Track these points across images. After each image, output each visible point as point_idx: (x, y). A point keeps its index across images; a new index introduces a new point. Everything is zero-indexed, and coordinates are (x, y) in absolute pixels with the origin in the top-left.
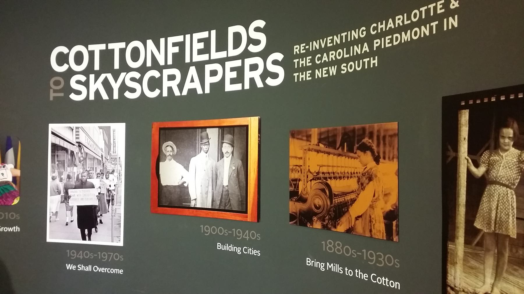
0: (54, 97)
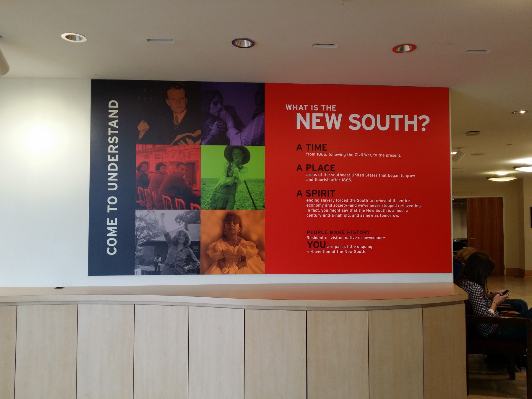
0: (110, 211)
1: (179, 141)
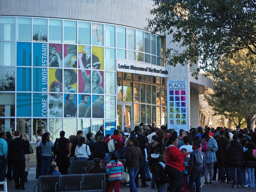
1: (88, 67)
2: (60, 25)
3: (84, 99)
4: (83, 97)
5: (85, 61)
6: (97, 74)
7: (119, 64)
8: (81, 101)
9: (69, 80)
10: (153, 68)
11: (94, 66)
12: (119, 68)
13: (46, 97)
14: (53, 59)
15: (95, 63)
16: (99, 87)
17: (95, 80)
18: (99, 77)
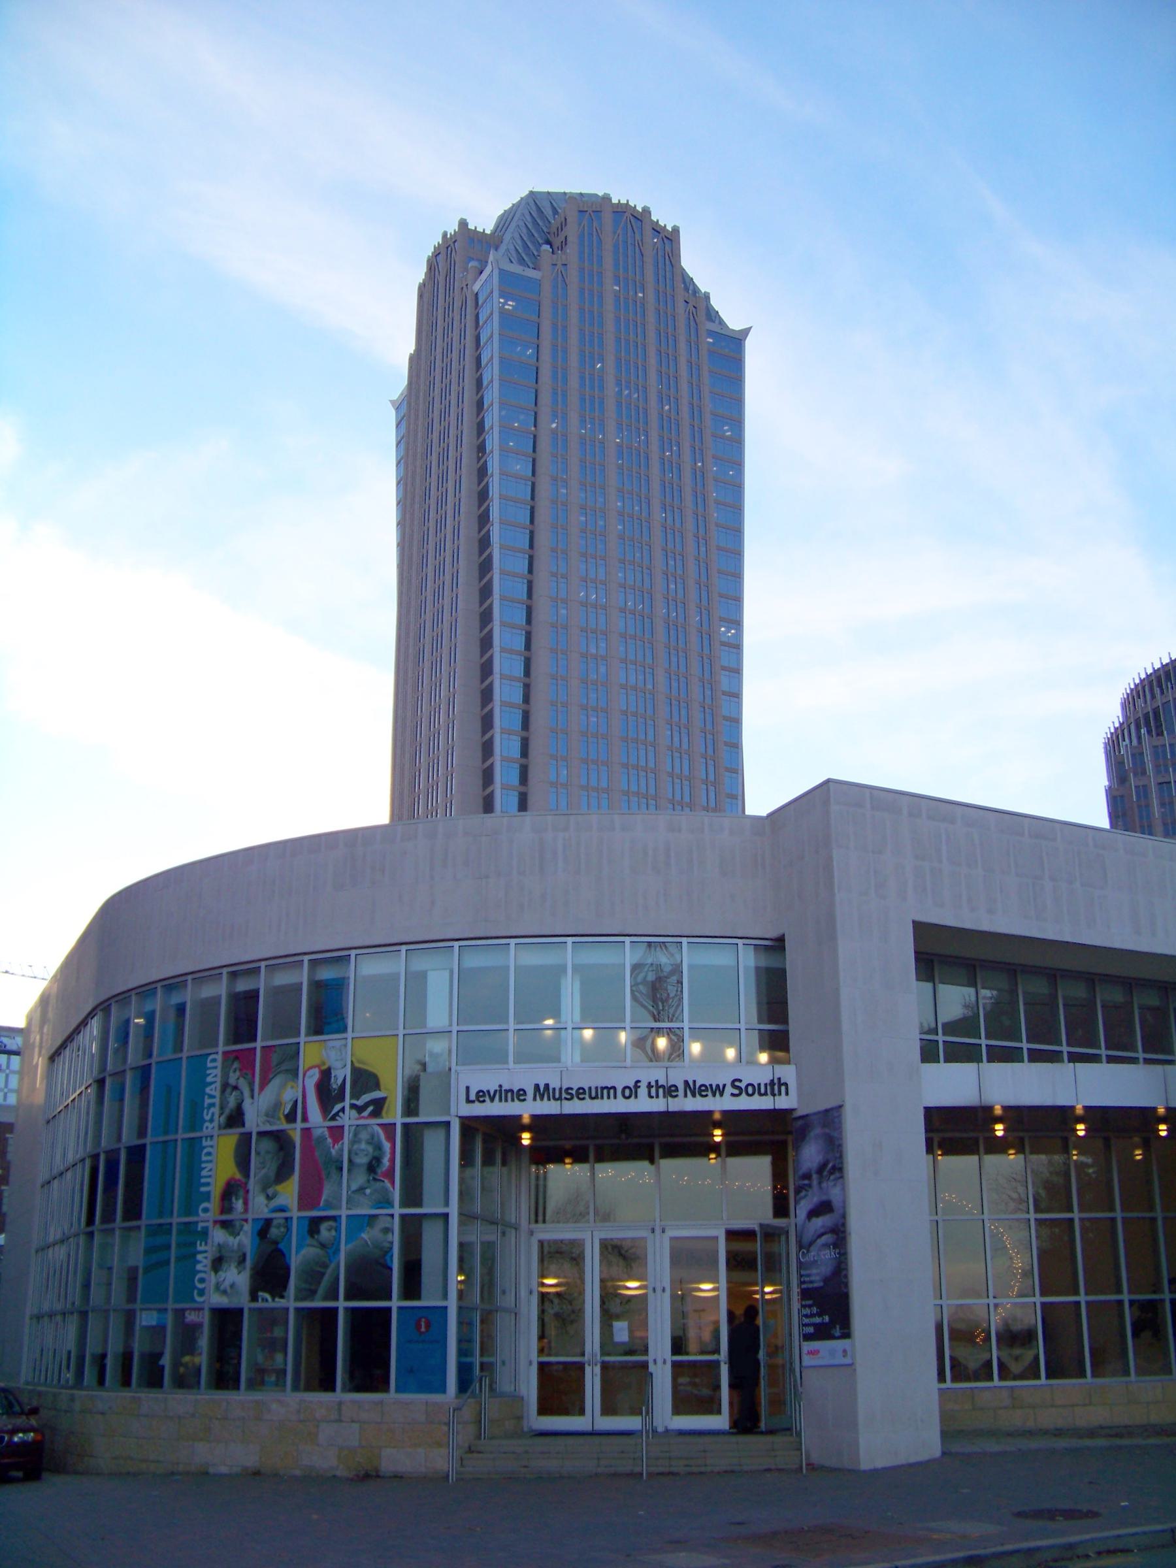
1: (337, 1114)
2: (733, 963)
3: (318, 1232)
4: (314, 1225)
5: (328, 1094)
6: (373, 1136)
7: (468, 1088)
8: (309, 1240)
9: (271, 1168)
10: (493, 1087)
11: (360, 1109)
12: (468, 1101)
13: (205, 1233)
14: (232, 1101)
15: (366, 1098)
16: (378, 1184)
17: (362, 1160)
18: (379, 1147)
